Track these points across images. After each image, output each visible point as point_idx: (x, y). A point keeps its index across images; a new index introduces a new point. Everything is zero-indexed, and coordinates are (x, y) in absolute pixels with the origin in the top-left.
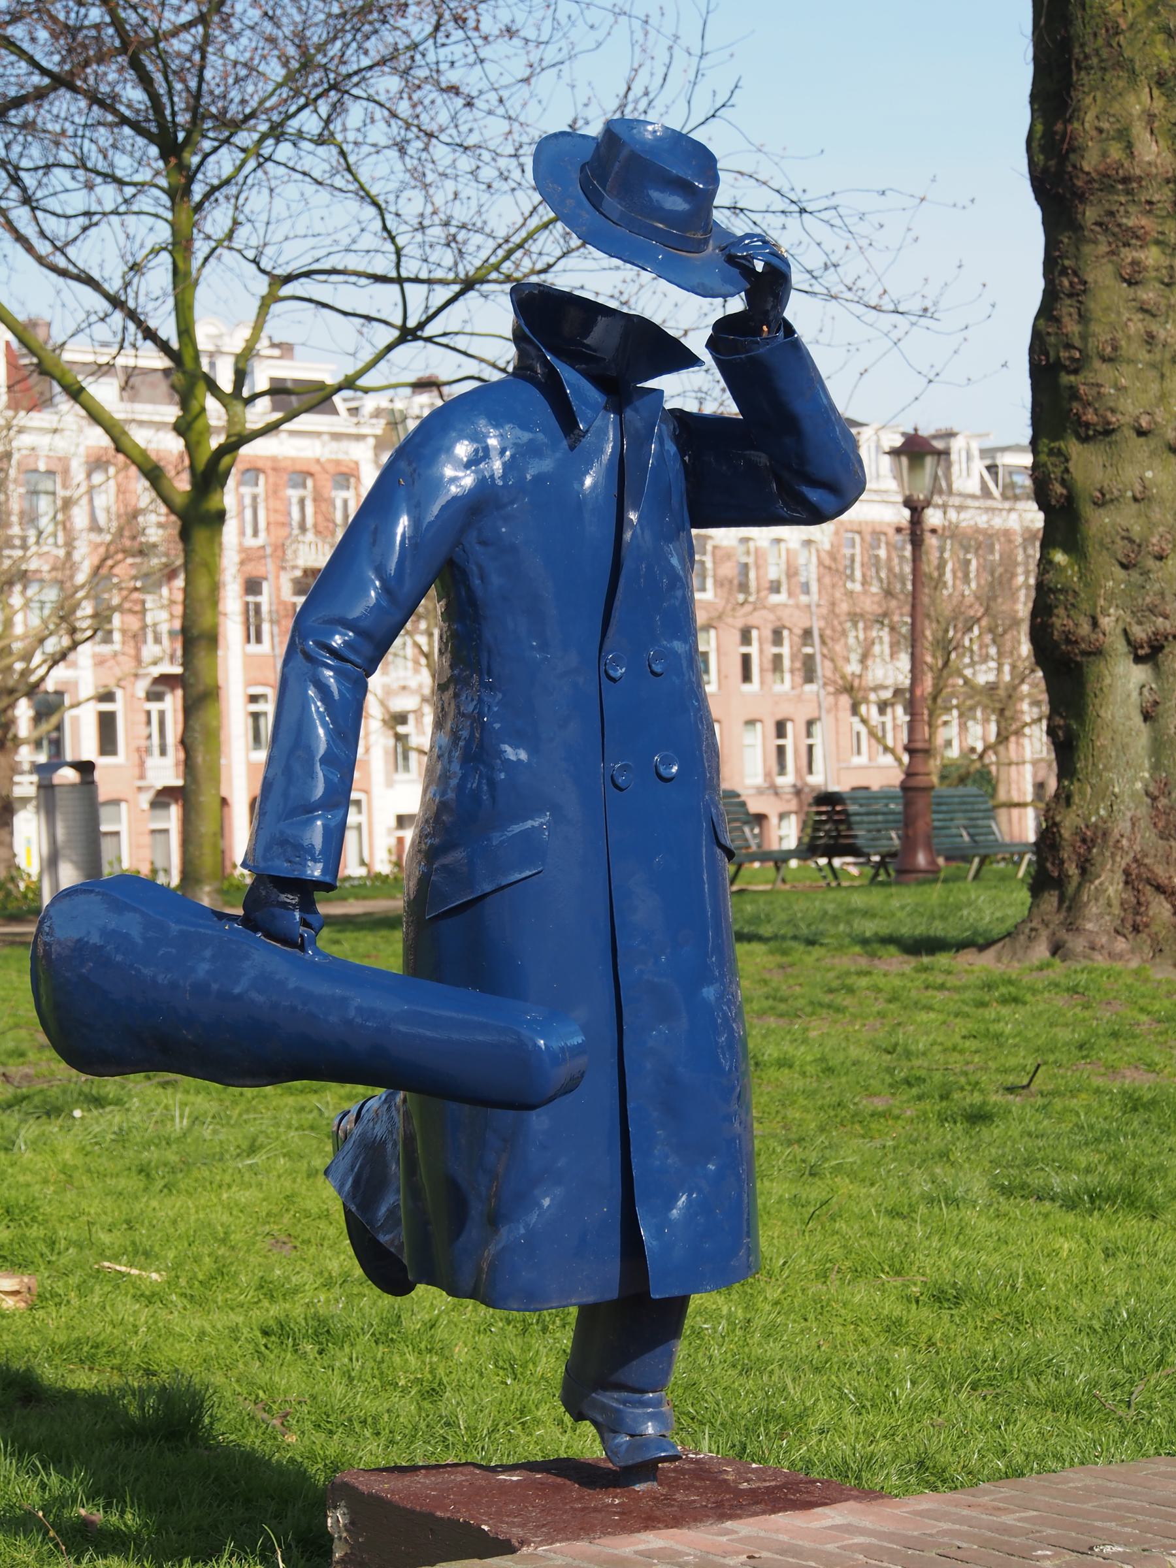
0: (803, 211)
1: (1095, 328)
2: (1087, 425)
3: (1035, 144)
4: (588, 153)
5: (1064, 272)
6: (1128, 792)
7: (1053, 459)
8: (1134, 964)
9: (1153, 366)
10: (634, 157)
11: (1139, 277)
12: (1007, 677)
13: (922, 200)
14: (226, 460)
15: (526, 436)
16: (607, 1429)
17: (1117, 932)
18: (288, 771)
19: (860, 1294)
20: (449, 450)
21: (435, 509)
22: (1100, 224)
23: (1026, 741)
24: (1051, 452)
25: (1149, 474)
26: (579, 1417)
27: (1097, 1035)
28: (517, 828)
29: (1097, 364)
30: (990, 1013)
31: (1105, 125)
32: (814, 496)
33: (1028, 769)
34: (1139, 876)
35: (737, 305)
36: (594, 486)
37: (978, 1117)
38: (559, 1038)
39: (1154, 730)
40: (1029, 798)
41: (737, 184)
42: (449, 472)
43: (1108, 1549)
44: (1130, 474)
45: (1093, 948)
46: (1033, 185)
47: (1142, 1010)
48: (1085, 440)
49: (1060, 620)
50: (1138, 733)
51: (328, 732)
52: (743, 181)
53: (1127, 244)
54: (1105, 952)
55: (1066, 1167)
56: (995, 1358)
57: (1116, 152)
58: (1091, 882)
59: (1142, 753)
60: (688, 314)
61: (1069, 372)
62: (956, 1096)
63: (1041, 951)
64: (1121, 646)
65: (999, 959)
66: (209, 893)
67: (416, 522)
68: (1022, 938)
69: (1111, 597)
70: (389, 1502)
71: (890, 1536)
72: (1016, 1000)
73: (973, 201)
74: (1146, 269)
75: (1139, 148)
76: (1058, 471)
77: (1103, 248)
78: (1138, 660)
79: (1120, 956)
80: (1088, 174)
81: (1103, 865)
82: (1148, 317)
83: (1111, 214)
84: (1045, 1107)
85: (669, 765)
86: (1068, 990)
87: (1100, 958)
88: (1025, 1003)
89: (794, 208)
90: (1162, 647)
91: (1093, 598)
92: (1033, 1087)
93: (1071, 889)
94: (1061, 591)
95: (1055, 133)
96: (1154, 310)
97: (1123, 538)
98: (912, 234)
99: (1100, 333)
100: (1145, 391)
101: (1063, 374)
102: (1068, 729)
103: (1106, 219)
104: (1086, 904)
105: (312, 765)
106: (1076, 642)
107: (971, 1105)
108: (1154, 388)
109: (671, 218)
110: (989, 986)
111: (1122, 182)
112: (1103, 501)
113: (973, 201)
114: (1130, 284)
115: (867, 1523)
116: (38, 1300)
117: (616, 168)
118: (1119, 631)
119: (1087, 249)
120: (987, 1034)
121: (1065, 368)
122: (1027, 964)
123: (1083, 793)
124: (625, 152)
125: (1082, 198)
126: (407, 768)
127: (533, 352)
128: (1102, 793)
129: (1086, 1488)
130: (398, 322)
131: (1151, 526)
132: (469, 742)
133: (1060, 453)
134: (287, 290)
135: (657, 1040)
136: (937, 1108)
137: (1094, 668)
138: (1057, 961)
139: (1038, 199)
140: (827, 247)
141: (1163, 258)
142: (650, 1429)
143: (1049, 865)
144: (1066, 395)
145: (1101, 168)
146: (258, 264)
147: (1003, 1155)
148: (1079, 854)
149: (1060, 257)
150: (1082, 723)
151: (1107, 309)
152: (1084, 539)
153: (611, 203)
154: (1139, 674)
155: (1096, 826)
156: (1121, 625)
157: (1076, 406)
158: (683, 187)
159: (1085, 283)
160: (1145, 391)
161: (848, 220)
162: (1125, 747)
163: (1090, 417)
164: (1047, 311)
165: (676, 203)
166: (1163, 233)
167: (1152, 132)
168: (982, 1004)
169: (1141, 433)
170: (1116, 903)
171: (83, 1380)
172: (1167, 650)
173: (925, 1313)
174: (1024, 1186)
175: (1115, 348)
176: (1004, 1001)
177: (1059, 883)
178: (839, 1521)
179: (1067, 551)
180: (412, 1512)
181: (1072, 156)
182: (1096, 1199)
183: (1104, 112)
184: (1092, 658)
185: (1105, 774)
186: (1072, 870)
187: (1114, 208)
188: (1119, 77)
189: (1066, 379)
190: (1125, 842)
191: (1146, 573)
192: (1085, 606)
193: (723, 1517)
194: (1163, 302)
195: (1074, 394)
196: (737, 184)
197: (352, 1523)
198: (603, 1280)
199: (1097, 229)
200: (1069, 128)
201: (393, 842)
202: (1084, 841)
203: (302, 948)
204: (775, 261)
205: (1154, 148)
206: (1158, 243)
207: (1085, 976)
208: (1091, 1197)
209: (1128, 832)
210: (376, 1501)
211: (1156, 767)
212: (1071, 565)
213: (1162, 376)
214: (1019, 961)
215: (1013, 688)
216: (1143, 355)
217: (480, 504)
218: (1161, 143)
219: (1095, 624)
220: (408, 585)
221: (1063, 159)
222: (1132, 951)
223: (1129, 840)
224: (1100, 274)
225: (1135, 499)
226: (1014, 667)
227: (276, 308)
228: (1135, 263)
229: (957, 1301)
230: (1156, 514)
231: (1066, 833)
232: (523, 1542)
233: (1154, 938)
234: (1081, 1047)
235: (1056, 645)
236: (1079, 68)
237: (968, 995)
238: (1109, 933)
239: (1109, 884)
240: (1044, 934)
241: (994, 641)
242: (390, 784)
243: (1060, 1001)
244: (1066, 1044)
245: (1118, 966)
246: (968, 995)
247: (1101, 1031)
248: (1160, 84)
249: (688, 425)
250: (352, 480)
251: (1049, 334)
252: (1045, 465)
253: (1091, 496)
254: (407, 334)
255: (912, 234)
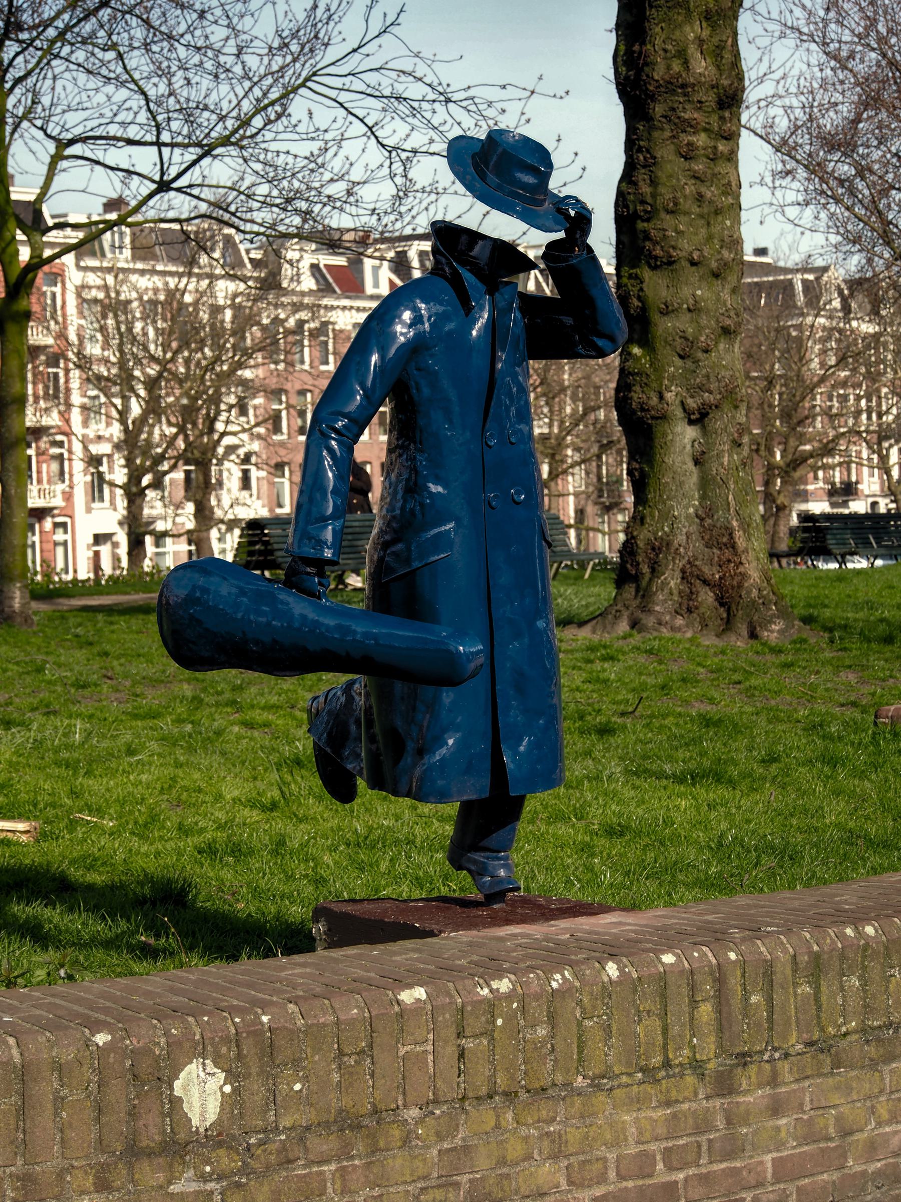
0: (448, 101)
1: (662, 190)
2: (656, 258)
3: (619, 59)
4: (477, 148)
5: (640, 150)
6: (683, 515)
7: (632, 281)
8: (689, 635)
9: (701, 216)
10: (505, 152)
11: (692, 154)
12: (556, 430)
13: (533, 92)
14: (30, 276)
15: (440, 309)
16: (477, 873)
17: (677, 612)
18: (311, 500)
19: (562, 830)
20: (400, 317)
21: (393, 351)
22: (665, 117)
23: (570, 478)
24: (630, 277)
25: (699, 292)
26: (459, 868)
27: (673, 681)
28: (436, 531)
29: (663, 215)
30: (598, 666)
31: (669, 47)
32: (600, 342)
33: (571, 499)
34: (691, 573)
35: (561, 235)
36: (478, 336)
37: (605, 731)
38: (469, 648)
39: (701, 471)
40: (572, 522)
41: (400, 80)
42: (399, 328)
43: (769, 929)
44: (686, 291)
45: (660, 624)
46: (617, 88)
47: (699, 664)
48: (654, 268)
49: (637, 395)
50: (691, 473)
51: (334, 475)
52: (403, 78)
53: (684, 131)
54: (668, 626)
55: (670, 759)
56: (656, 861)
57: (676, 67)
58: (659, 578)
59: (694, 488)
60: (532, 241)
61: (643, 221)
62: (589, 718)
63: (623, 626)
64: (679, 413)
65: (594, 632)
66: (20, 589)
67: (382, 358)
68: (610, 616)
69: (672, 378)
70: (354, 916)
71: (646, 926)
72: (612, 658)
73: (567, 93)
74: (697, 148)
75: (692, 63)
76: (635, 289)
77: (668, 134)
78: (691, 422)
79: (679, 629)
80: (657, 81)
81: (667, 566)
82: (698, 182)
83: (673, 109)
84: (648, 725)
85: (519, 495)
86: (646, 651)
87: (665, 630)
88: (619, 661)
89: (442, 98)
90: (707, 414)
91: (660, 379)
92: (637, 713)
93: (644, 583)
94: (637, 374)
95: (634, 52)
96: (703, 177)
97: (681, 337)
98: (524, 118)
99: (666, 194)
100: (696, 234)
101: (639, 221)
102: (642, 471)
103: (669, 113)
104: (655, 593)
105: (326, 495)
106: (648, 410)
107: (600, 723)
108: (703, 231)
109: (524, 186)
110: (592, 649)
111: (680, 87)
112: (667, 311)
113: (567, 93)
114: (686, 159)
115: (630, 921)
116: (42, 836)
117: (494, 159)
118: (677, 402)
119: (656, 134)
120: (598, 680)
121: (640, 218)
122: (614, 635)
123: (653, 515)
124: (500, 150)
125: (653, 98)
126: (102, 499)
127: (444, 260)
128: (666, 515)
129: (747, 905)
130: (157, 178)
131: (700, 329)
132: (408, 480)
133: (636, 277)
134: (69, 151)
135: (513, 649)
136: (577, 725)
137: (659, 428)
138: (635, 632)
139: (621, 97)
140: (464, 126)
141: (709, 141)
142: (502, 873)
143: (629, 566)
144: (641, 236)
145: (667, 77)
146: (45, 132)
147: (627, 753)
148: (650, 559)
149: (638, 140)
150: (652, 467)
151: (670, 176)
152: (654, 338)
153: (491, 177)
154: (690, 433)
155: (662, 539)
156: (679, 398)
157: (648, 245)
158: (534, 171)
159: (655, 158)
160: (696, 234)
161: (481, 107)
162: (681, 484)
163: (658, 252)
164: (628, 176)
165: (529, 179)
166: (709, 123)
167: (702, 53)
168: (589, 661)
169: (693, 263)
170: (675, 592)
171: (96, 878)
172: (711, 416)
173: (603, 841)
174: (646, 771)
175: (676, 204)
176: (604, 659)
177: (636, 579)
178: (614, 920)
179: (641, 346)
180: (370, 920)
181: (646, 69)
182: (694, 777)
183: (668, 38)
184: (659, 421)
185: (668, 502)
186: (645, 569)
187: (675, 105)
188: (679, 14)
189: (641, 225)
190: (682, 550)
191: (696, 362)
192: (654, 385)
193: (548, 919)
194: (709, 171)
195: (647, 236)
196: (400, 80)
197: (329, 930)
198: (477, 788)
199: (664, 120)
200: (644, 49)
201: (91, 554)
202: (653, 549)
203: (319, 598)
204: (584, 212)
205: (703, 64)
206: (705, 130)
207: (657, 642)
208: (692, 777)
209: (684, 543)
210: (347, 916)
211: (703, 498)
212: (644, 356)
213: (708, 224)
214: (609, 633)
215: (560, 440)
216: (695, 209)
217: (416, 348)
218: (708, 60)
219: (661, 397)
220: (378, 393)
221: (639, 71)
222: (687, 626)
223: (685, 548)
224: (665, 152)
225: (689, 310)
226: (562, 422)
227: (64, 164)
228: (690, 144)
229: (622, 834)
230: (704, 321)
231: (641, 544)
232: (441, 932)
233: (702, 618)
234: (663, 688)
235: (634, 412)
236: (651, 7)
237: (578, 655)
238: (670, 613)
239: (672, 580)
240: (626, 614)
241: (547, 403)
242: (89, 510)
243: (642, 659)
244: (653, 686)
245: (678, 636)
246: (578, 655)
247: (675, 677)
248: (707, 19)
249: (531, 302)
250: (59, 279)
251: (629, 193)
252: (626, 285)
253: (659, 308)
254: (163, 186)
255: (524, 118)
